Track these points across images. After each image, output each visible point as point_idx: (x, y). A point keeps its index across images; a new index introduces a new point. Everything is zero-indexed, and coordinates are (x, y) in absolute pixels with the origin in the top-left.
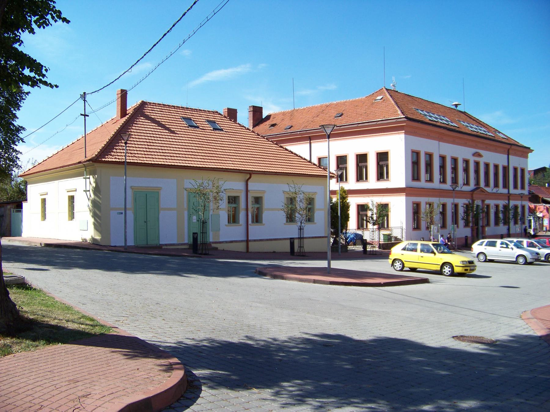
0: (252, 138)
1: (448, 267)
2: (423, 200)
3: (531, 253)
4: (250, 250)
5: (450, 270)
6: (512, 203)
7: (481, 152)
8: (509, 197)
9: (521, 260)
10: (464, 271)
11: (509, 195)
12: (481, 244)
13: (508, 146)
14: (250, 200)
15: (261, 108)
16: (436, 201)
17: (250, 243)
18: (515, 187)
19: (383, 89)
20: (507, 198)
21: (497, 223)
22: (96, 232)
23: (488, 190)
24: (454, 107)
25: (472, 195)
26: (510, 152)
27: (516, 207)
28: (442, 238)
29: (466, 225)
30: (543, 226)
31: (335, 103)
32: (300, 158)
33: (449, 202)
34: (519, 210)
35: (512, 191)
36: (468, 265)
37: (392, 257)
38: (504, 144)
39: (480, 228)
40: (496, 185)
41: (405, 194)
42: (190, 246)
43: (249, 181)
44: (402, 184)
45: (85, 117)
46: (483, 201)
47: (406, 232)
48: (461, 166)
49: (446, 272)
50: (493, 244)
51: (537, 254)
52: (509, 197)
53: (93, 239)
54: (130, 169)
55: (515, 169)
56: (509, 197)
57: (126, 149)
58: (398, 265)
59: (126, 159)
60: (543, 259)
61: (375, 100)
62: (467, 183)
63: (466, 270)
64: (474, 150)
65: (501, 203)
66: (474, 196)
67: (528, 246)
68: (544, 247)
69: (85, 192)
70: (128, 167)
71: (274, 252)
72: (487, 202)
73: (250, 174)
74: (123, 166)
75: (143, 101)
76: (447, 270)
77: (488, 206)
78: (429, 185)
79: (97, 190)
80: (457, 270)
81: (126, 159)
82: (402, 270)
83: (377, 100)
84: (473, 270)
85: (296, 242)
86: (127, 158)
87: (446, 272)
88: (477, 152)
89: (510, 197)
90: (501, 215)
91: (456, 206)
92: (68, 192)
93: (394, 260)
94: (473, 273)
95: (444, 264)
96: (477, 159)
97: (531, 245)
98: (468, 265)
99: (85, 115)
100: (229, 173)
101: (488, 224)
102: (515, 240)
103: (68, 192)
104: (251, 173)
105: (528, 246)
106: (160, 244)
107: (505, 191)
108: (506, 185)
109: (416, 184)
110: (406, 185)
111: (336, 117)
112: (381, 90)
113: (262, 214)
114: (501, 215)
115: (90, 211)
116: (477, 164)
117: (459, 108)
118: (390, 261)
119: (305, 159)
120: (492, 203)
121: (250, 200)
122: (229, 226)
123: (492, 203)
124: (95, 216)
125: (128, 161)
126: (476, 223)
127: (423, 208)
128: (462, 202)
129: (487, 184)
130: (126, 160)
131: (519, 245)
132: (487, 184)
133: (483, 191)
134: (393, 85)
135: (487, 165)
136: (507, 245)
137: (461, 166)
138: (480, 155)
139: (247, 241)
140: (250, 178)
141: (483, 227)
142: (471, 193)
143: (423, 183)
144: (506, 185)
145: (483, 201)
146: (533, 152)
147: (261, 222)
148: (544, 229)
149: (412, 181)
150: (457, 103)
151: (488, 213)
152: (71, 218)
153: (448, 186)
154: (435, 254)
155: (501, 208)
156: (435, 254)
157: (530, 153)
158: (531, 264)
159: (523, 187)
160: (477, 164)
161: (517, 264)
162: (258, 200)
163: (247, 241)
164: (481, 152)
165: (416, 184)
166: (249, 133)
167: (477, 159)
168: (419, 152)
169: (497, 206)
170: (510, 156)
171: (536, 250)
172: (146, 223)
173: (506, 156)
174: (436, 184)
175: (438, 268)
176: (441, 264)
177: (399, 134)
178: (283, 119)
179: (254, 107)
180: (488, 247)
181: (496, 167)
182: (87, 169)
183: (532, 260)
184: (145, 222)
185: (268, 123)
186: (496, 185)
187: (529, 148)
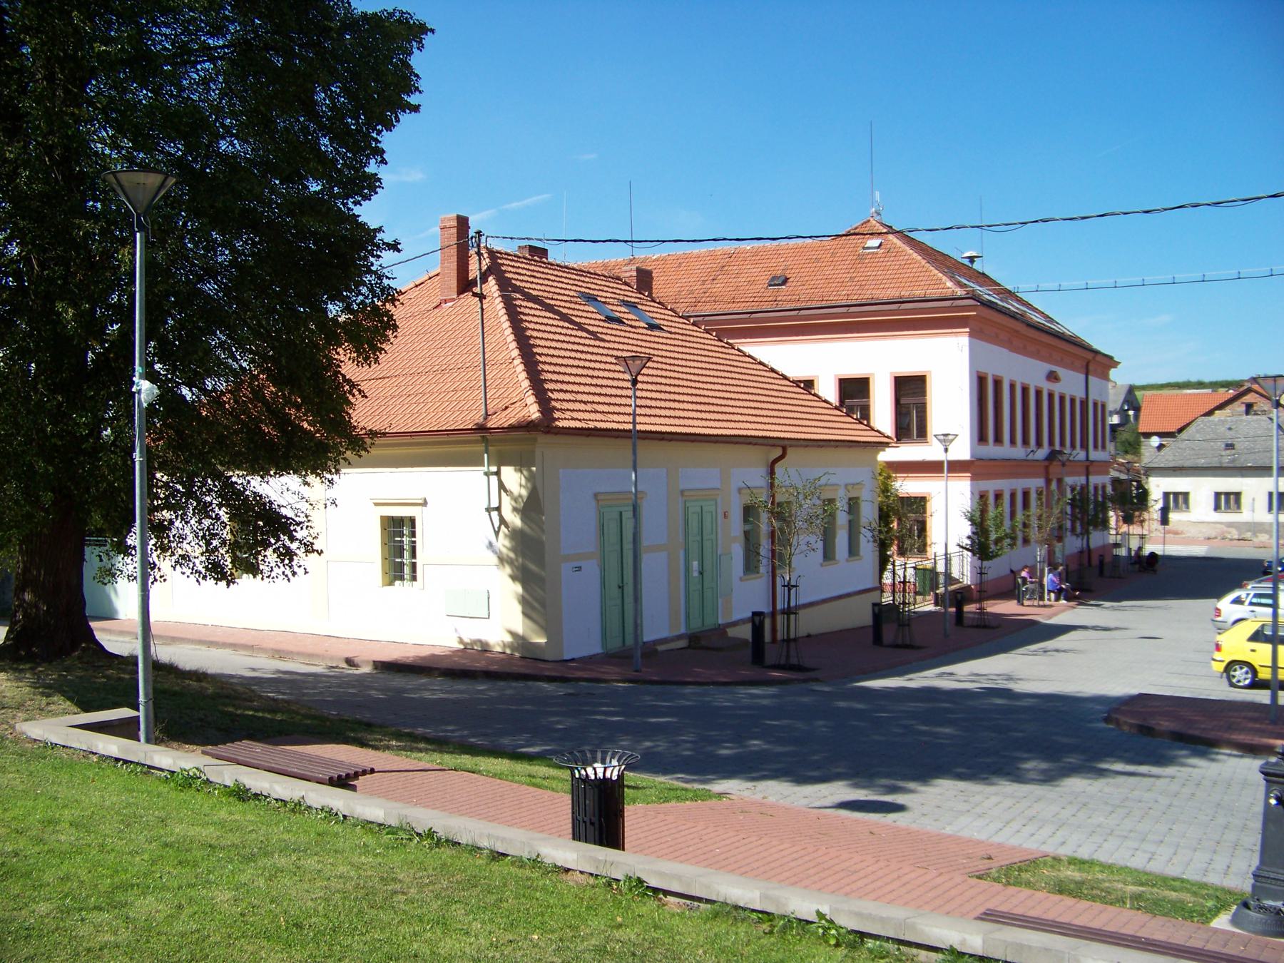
0: (706, 347)
1: (1238, 669)
5: (1245, 669)
7: (1061, 372)
8: (1087, 468)
11: (1088, 463)
12: (1238, 601)
19: (869, 221)
20: (1084, 470)
22: (528, 622)
24: (966, 262)
25: (1047, 468)
26: (1091, 368)
31: (748, 248)
32: (816, 399)
38: (1085, 352)
41: (969, 475)
42: (690, 642)
43: (777, 465)
44: (962, 450)
45: (1275, 381)
47: (971, 563)
49: (1242, 678)
53: (520, 642)
54: (645, 449)
55: (1095, 404)
56: (1087, 468)
57: (637, 397)
58: (1240, 674)
59: (634, 423)
61: (864, 248)
64: (1048, 367)
69: (487, 513)
70: (639, 443)
73: (784, 449)
74: (629, 443)
75: (547, 250)
79: (531, 507)
81: (634, 423)
83: (869, 248)
86: (639, 419)
87: (1242, 678)
89: (1091, 469)
92: (376, 504)
93: (1231, 665)
100: (737, 446)
103: (376, 504)
104: (784, 446)
106: (644, 643)
109: (991, 450)
110: (972, 456)
111: (770, 285)
112: (865, 223)
115: (502, 560)
116: (1051, 396)
117: (977, 266)
118: (1221, 666)
119: (826, 401)
122: (747, 580)
124: (522, 576)
125: (639, 427)
130: (634, 426)
134: (876, 212)
135: (1062, 398)
142: (1046, 463)
144: (1084, 446)
146: (1119, 366)
149: (979, 445)
150: (974, 254)
152: (387, 580)
157: (1113, 370)
164: (1061, 372)
165: (991, 450)
166: (698, 334)
168: (984, 375)
170: (1090, 378)
172: (620, 590)
173: (1082, 377)
176: (1227, 661)
177: (957, 336)
181: (1073, 401)
182: (490, 448)
184: (620, 587)
187: (1111, 358)
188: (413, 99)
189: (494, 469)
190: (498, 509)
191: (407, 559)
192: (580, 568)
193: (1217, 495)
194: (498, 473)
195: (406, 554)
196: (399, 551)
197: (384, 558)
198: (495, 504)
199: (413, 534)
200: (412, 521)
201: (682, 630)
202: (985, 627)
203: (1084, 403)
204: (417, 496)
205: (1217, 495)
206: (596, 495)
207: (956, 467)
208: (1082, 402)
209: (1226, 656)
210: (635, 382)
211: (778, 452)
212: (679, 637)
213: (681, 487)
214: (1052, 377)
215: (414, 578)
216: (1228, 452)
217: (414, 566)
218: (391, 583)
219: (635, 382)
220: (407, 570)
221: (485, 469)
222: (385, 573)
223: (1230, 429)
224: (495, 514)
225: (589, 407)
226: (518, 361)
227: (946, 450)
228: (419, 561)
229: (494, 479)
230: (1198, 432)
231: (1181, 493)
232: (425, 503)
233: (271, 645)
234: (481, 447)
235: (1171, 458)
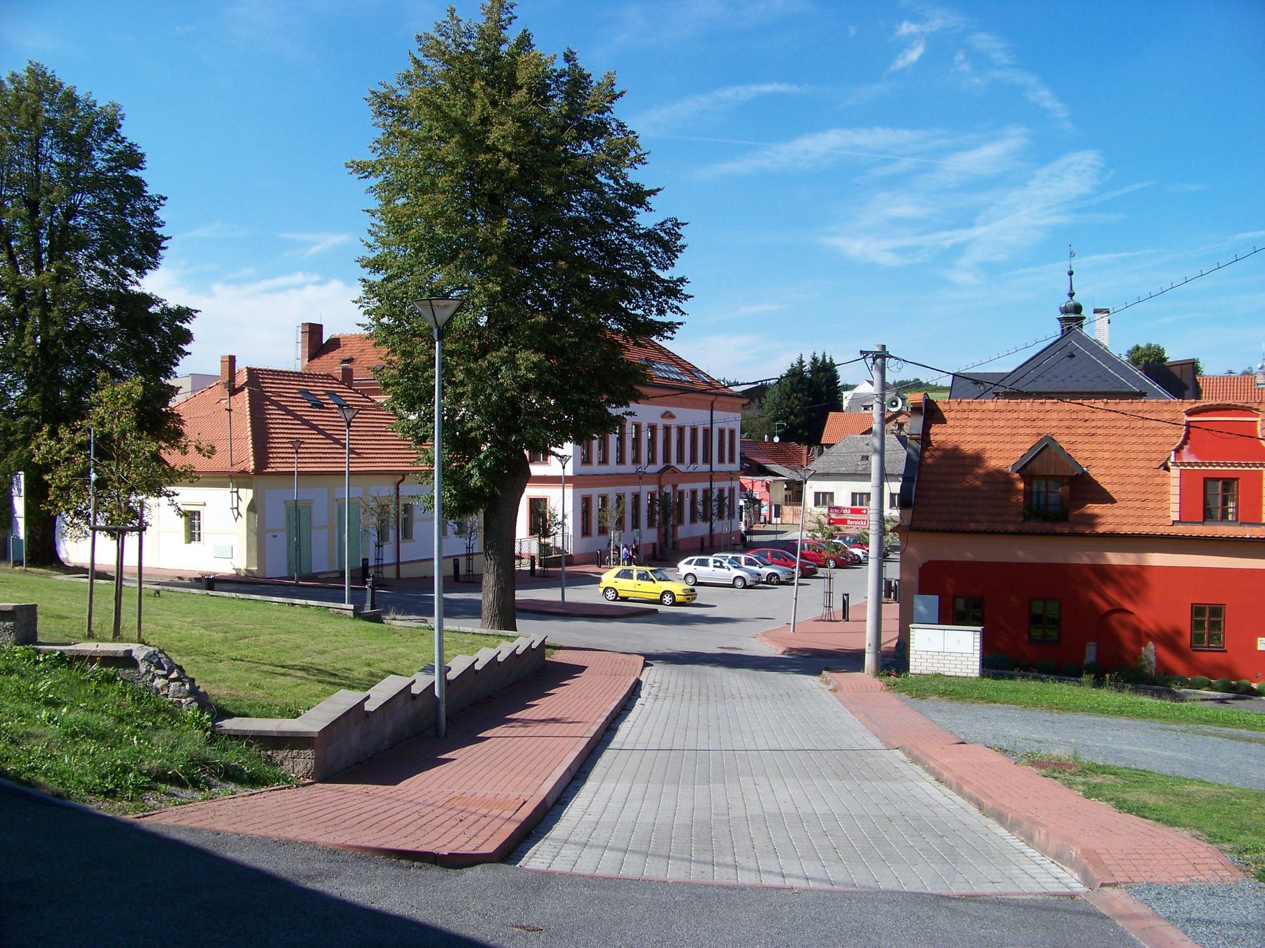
2: (595, 492)
3: (752, 573)
4: (402, 575)
6: (717, 485)
7: (674, 410)
8: (711, 476)
9: (739, 583)
10: (685, 600)
12: (689, 563)
13: (712, 398)
14: (401, 508)
15: (322, 326)
16: (611, 492)
17: (402, 567)
18: (721, 460)
20: (709, 478)
21: (693, 520)
23: (682, 468)
25: (660, 478)
27: (721, 491)
28: (625, 549)
29: (651, 524)
30: (760, 514)
33: (628, 491)
34: (726, 494)
35: (717, 466)
36: (690, 593)
37: (603, 585)
39: (670, 529)
40: (694, 460)
46: (675, 487)
48: (646, 435)
50: (704, 563)
51: (759, 575)
52: (711, 476)
55: (722, 432)
56: (711, 476)
58: (610, 594)
60: (765, 580)
62: (652, 461)
63: (688, 599)
64: (663, 409)
65: (700, 487)
66: (663, 479)
67: (746, 564)
68: (766, 565)
71: (425, 577)
72: (680, 487)
76: (667, 599)
77: (681, 494)
78: (603, 469)
80: (678, 599)
82: (615, 600)
84: (694, 599)
85: (462, 562)
88: (667, 412)
89: (714, 477)
90: (700, 508)
91: (637, 497)
93: (606, 588)
94: (694, 602)
95: (664, 592)
96: (668, 422)
97: (750, 562)
98: (690, 593)
99: (230, 410)
101: (681, 521)
102: (730, 556)
104: (404, 474)
105: (746, 564)
107: (706, 468)
108: (707, 459)
113: (412, 525)
114: (700, 508)
116: (667, 429)
118: (601, 590)
120: (686, 487)
121: (401, 508)
123: (686, 487)
126: (665, 521)
127: (596, 504)
128: (646, 490)
129: (680, 460)
131: (735, 563)
132: (680, 460)
133: (675, 471)
135: (681, 430)
136: (721, 563)
137: (646, 435)
138: (672, 416)
139: (398, 563)
140: (403, 480)
141: (674, 526)
143: (595, 468)
144: (707, 459)
145: (675, 487)
147: (411, 538)
148: (762, 520)
151: (680, 505)
153: (629, 468)
154: (654, 582)
155: (700, 497)
156: (654, 582)
158: (750, 587)
159: (732, 460)
160: (667, 429)
161: (735, 587)
162: (408, 508)
163: (398, 563)
164: (674, 410)
165: (587, 469)
167: (668, 422)
169: (694, 493)
171: (756, 569)
174: (612, 467)
175: (658, 597)
178: (362, 351)
179: (311, 325)
180: (697, 567)
181: (694, 431)
183: (752, 583)
185: (336, 355)
186: (694, 460)
188: (186, 348)
189: (235, 490)
190: (237, 508)
191: (197, 531)
192: (276, 536)
193: (854, 495)
194: (237, 492)
195: (702, 528)
196: (193, 527)
197: (186, 531)
198: (235, 506)
199: (199, 519)
200: (199, 512)
201: (337, 568)
202: (547, 577)
203: (708, 433)
204: (201, 501)
205: (854, 495)
206: (285, 502)
207: (568, 480)
208: (705, 431)
209: (603, 585)
210: (349, 426)
211: (401, 478)
212: (334, 572)
213: (336, 497)
214: (668, 415)
215: (199, 540)
216: (863, 462)
217: (199, 534)
218: (189, 542)
219: (349, 426)
220: (196, 536)
221: (230, 489)
222: (186, 537)
223: (867, 444)
224: (235, 511)
225: (284, 460)
226: (250, 438)
227: (564, 467)
228: (202, 532)
229: (235, 494)
230: (844, 446)
231: (865, 494)
232: (205, 505)
233: (131, 571)
234: (229, 480)
235: (821, 467)
